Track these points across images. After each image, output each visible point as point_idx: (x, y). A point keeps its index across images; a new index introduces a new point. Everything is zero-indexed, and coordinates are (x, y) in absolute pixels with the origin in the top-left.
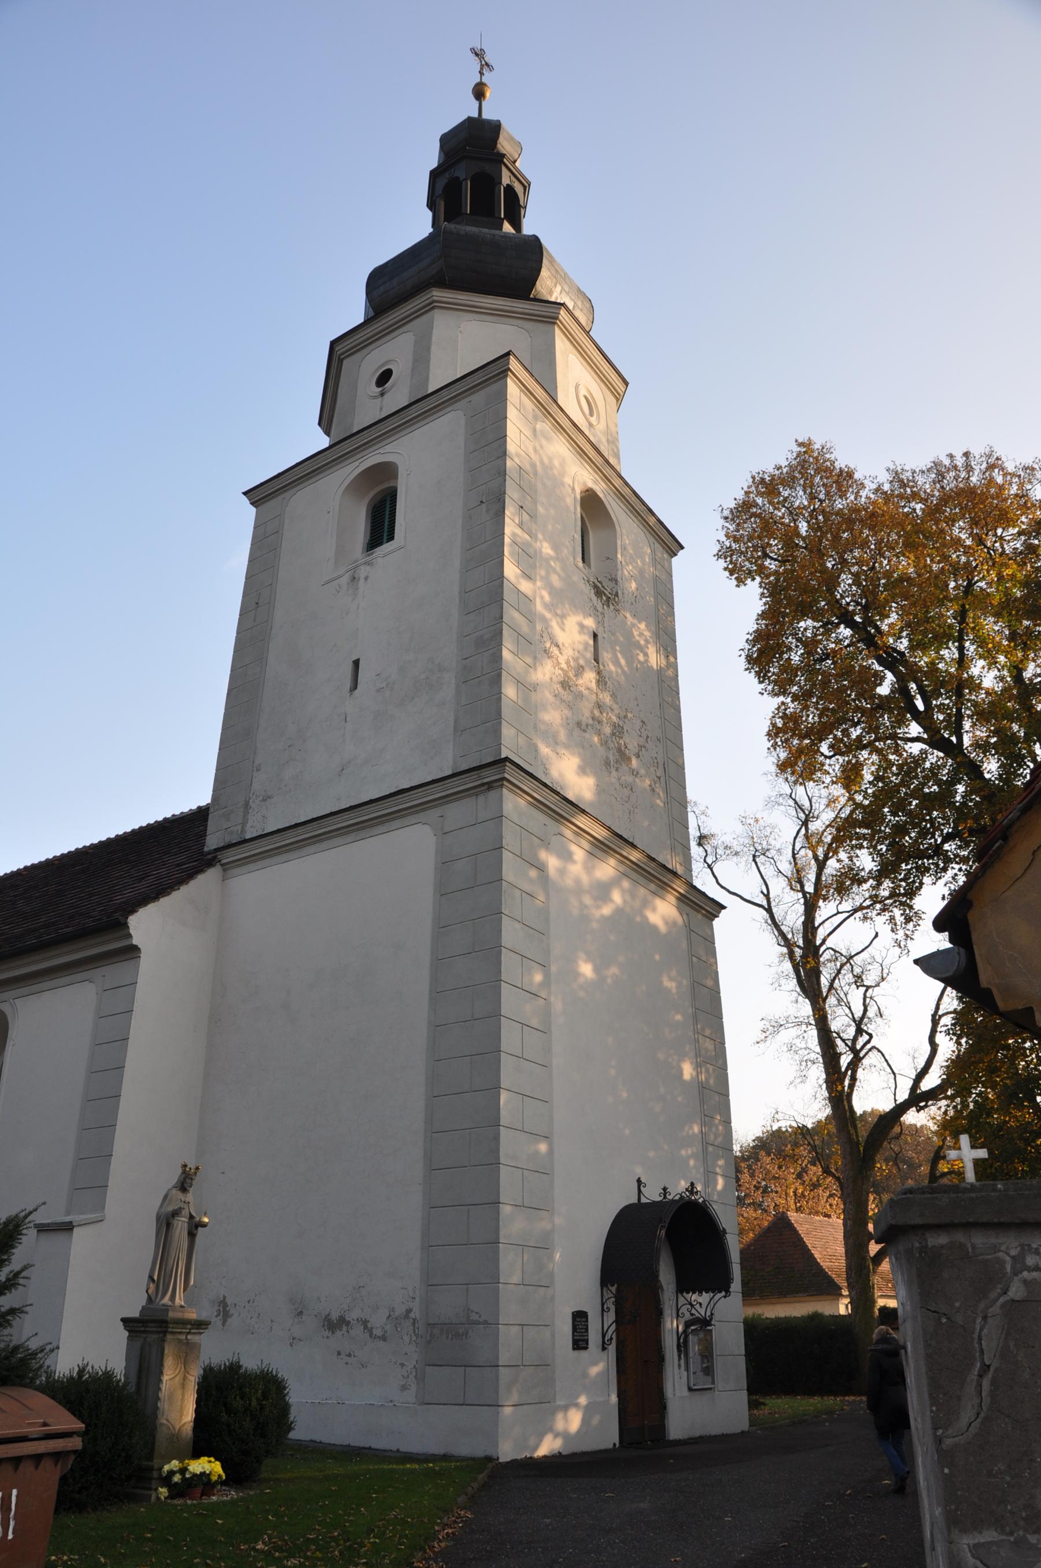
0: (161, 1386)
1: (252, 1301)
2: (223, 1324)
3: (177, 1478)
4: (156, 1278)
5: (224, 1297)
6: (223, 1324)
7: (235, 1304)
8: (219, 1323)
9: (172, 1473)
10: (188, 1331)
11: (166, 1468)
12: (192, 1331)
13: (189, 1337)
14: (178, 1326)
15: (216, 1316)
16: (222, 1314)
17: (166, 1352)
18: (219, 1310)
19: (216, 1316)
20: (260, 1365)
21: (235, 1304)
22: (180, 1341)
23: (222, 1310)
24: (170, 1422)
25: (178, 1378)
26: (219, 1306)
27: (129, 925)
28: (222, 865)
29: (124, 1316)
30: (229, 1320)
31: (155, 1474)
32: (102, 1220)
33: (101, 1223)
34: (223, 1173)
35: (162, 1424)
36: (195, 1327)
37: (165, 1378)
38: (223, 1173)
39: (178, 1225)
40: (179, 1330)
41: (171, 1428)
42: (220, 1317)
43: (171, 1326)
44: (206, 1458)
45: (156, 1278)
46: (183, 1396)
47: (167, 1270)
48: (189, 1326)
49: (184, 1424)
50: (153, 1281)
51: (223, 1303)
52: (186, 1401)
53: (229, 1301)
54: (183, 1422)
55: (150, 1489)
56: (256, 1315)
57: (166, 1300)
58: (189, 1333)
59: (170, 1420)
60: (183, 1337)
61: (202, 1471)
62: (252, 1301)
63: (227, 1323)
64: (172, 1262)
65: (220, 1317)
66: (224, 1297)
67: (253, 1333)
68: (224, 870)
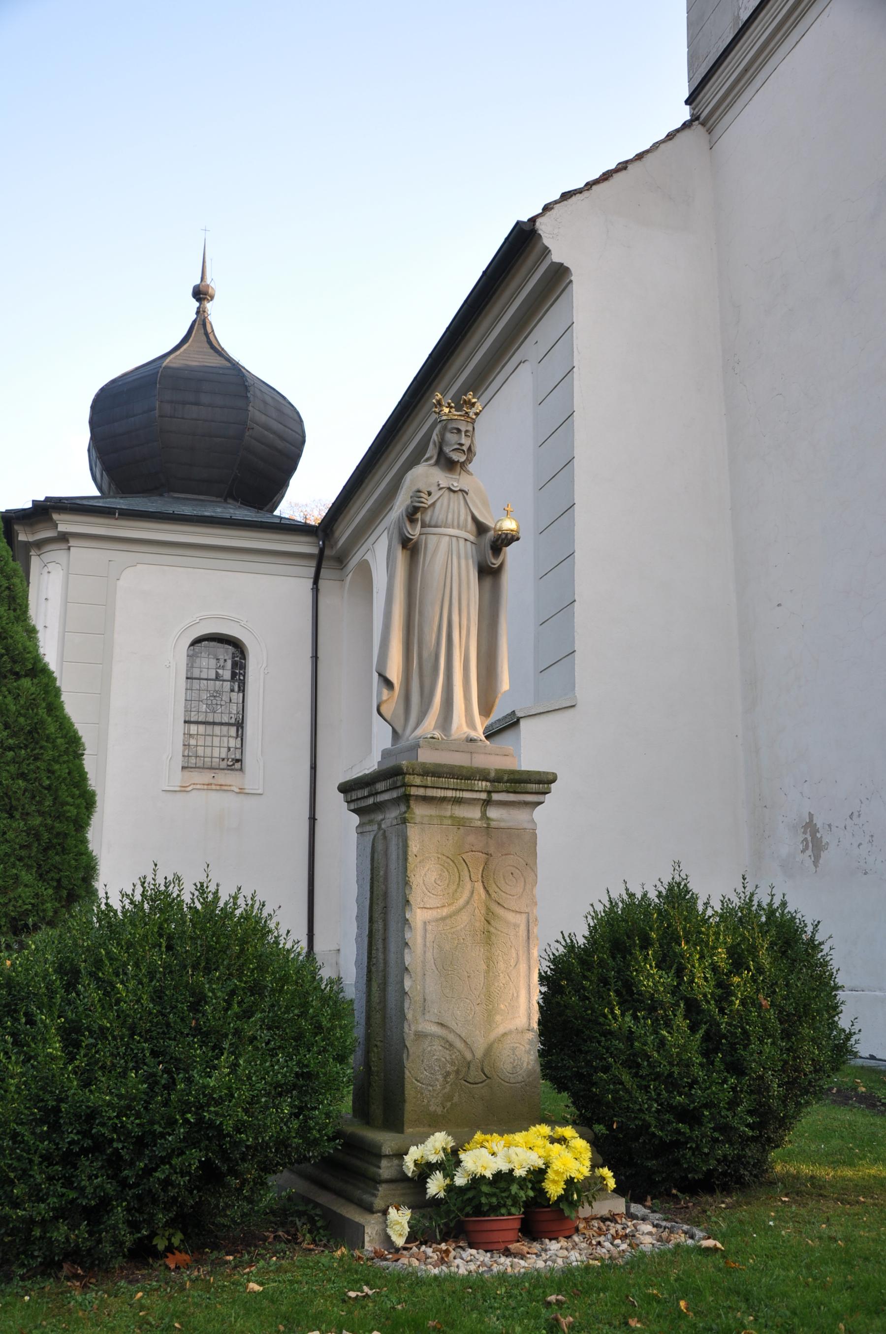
0: (408, 935)
1: (856, 814)
2: (816, 863)
3: (436, 1185)
4: (394, 673)
5: (811, 815)
6: (816, 863)
7: (830, 826)
8: (809, 862)
9: (426, 1169)
10: (484, 796)
11: (414, 1154)
12: (495, 797)
13: (493, 813)
14: (442, 781)
15: (803, 852)
16: (810, 845)
17: (414, 847)
18: (806, 839)
19: (803, 852)
20: (740, 889)
21: (830, 826)
22: (460, 823)
23: (809, 839)
24: (451, 1030)
25: (464, 918)
26: (805, 833)
27: (540, 232)
28: (703, 124)
29: (342, 780)
30: (823, 855)
31: (386, 1169)
32: (573, 706)
33: (571, 711)
34: (779, 605)
35: (420, 1036)
36: (501, 786)
37: (418, 916)
38: (779, 605)
39: (437, 546)
40: (450, 794)
41: (459, 1044)
42: (809, 852)
43: (418, 780)
44: (545, 1129)
45: (394, 673)
46: (489, 960)
47: (425, 655)
48: (484, 785)
49: (504, 1035)
50: (388, 684)
51: (810, 827)
52: (503, 979)
53: (819, 821)
54: (501, 1030)
55: (369, 1209)
56: (868, 838)
57: (429, 726)
58: (487, 803)
59: (452, 1024)
60: (474, 813)
61: (505, 1168)
62: (856, 814)
63: (821, 861)
64: (434, 636)
65: (809, 852)
66: (811, 815)
67: (866, 873)
68: (710, 131)
